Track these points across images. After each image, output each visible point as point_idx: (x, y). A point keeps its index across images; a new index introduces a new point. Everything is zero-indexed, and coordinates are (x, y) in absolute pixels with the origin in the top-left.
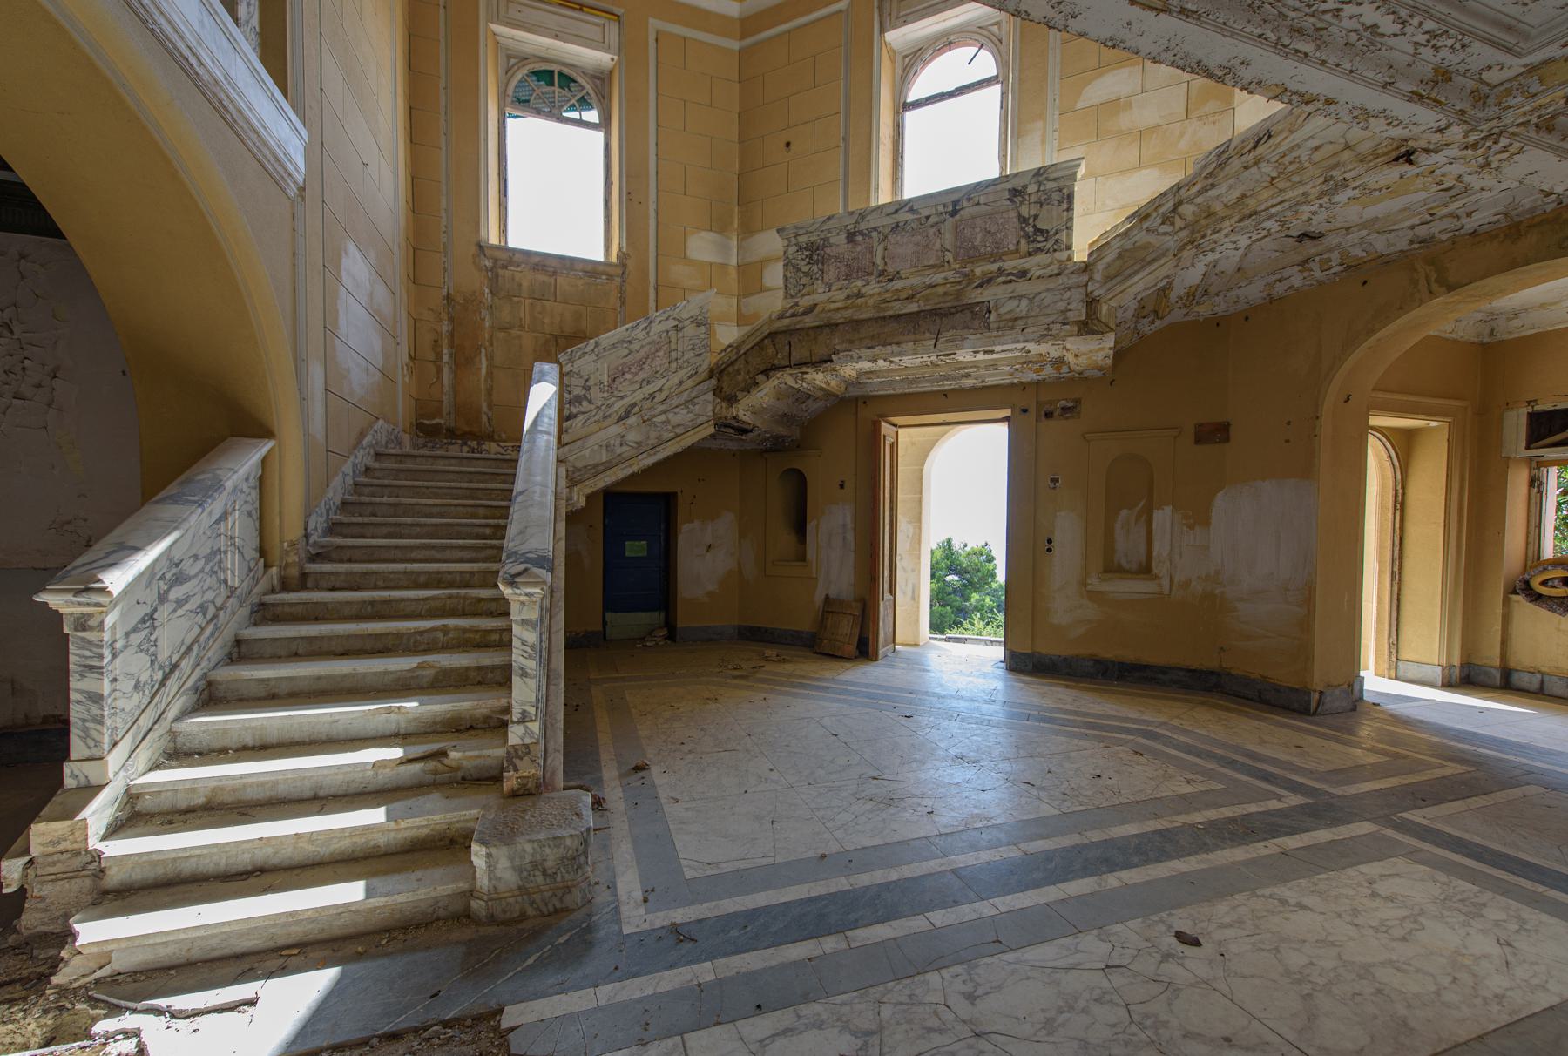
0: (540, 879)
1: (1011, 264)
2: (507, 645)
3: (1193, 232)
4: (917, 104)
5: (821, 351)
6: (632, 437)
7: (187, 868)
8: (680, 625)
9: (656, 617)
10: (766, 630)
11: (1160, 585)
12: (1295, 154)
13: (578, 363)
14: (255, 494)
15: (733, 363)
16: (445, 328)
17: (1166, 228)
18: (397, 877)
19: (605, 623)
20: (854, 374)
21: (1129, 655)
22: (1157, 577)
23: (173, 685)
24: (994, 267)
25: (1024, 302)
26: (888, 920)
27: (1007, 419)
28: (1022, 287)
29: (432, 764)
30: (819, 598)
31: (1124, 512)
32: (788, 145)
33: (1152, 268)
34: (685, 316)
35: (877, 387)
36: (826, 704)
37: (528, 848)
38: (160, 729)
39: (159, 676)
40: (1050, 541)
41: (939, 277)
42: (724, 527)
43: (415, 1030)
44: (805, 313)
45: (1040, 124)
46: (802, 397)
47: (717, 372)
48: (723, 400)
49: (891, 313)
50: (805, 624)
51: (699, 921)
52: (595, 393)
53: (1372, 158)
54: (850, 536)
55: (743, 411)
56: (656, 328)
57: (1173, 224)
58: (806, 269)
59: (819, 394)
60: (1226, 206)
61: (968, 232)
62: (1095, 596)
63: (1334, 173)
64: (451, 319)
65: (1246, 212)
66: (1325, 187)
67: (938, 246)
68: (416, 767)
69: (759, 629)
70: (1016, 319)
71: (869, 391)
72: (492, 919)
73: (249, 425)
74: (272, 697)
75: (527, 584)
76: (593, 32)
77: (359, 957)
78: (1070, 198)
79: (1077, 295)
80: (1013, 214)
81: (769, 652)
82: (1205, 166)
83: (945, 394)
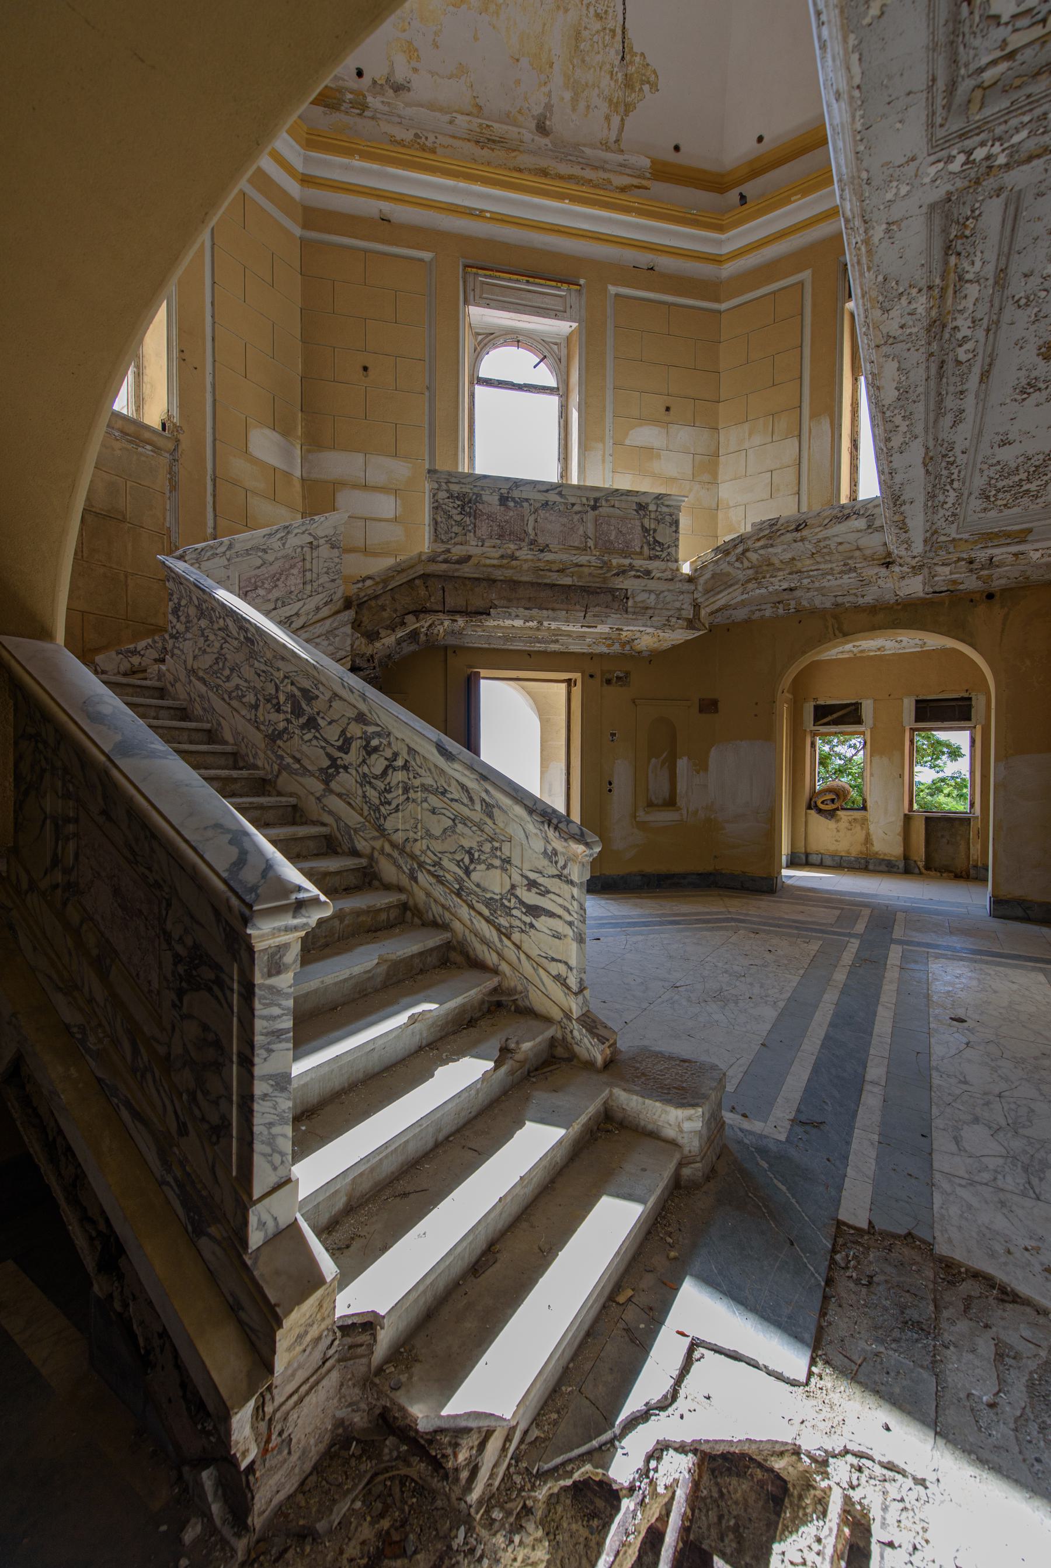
1: (638, 563)
3: (757, 573)
4: (488, 382)
5: (477, 603)
11: (681, 815)
12: (827, 542)
17: (737, 564)
21: (662, 868)
22: (679, 809)
24: (627, 562)
27: (569, 681)
28: (652, 585)
31: (653, 760)
33: (731, 590)
34: (320, 533)
40: (610, 784)
41: (583, 559)
45: (600, 445)
49: (548, 581)
53: (870, 559)
57: (742, 563)
58: (458, 518)
60: (781, 561)
61: (605, 527)
62: (642, 826)
63: (850, 562)
65: (794, 569)
66: (844, 568)
67: (581, 532)
70: (647, 608)
79: (687, 599)
80: (638, 523)
82: (761, 530)
83: (529, 654)
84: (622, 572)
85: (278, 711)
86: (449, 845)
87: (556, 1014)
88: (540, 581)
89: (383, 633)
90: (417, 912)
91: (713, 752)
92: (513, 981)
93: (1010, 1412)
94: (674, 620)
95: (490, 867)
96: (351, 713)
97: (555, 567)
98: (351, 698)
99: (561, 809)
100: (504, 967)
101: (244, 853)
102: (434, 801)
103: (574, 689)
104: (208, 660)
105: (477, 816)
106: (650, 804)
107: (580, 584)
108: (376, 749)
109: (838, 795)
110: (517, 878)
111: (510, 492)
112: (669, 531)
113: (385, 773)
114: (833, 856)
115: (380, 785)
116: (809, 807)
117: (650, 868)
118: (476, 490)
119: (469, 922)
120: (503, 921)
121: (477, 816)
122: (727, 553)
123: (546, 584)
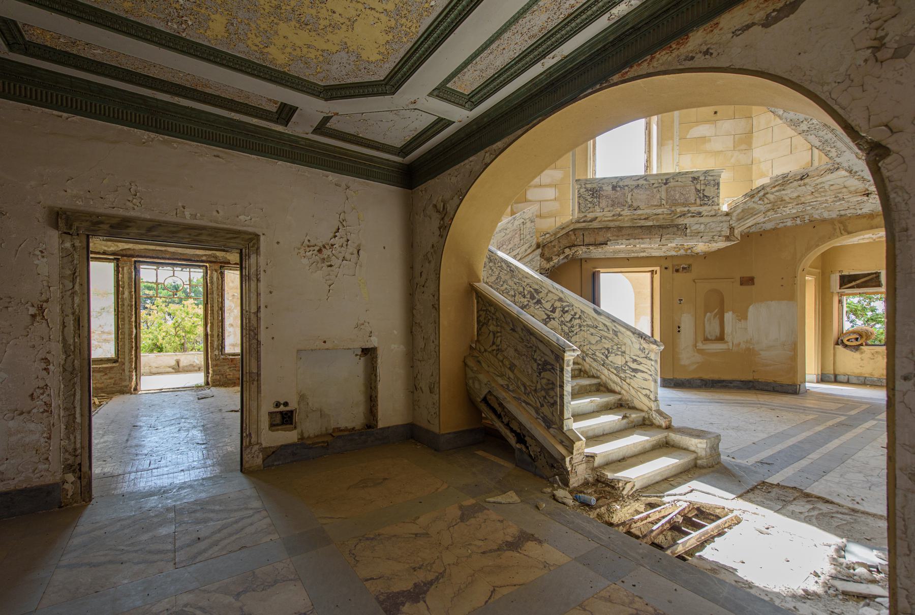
1: (693, 209)
5: (601, 239)
17: (760, 202)
21: (716, 377)
24: (686, 209)
25: (703, 226)
28: (702, 220)
41: (659, 211)
44: (591, 221)
45: (671, 142)
61: (672, 193)
62: (700, 351)
67: (658, 197)
78: (718, 184)
79: (726, 225)
80: (693, 187)
84: (683, 215)
85: (524, 297)
86: (599, 347)
87: (646, 409)
90: (586, 372)
91: (751, 309)
92: (626, 396)
94: (716, 238)
95: (616, 355)
96: (556, 298)
97: (643, 217)
98: (557, 292)
99: (649, 333)
100: (623, 392)
101: (558, 339)
102: (592, 330)
103: (655, 276)
104: (493, 279)
105: (611, 335)
106: (706, 339)
108: (567, 311)
109: (861, 336)
110: (628, 359)
111: (617, 184)
112: (713, 189)
113: (571, 320)
114: (858, 377)
115: (569, 325)
116: (837, 344)
117: (706, 376)
119: (607, 375)
120: (622, 375)
121: (611, 335)
122: (752, 196)
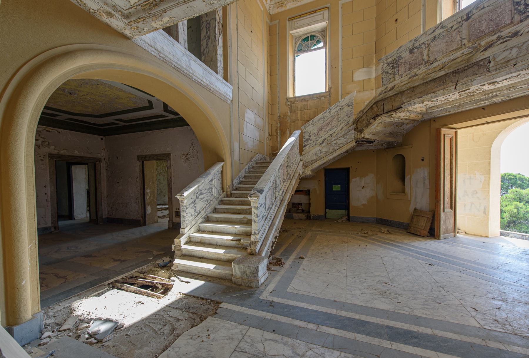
0: (246, 276)
2: (250, 214)
5: (397, 104)
6: (324, 150)
7: (193, 253)
8: (351, 215)
9: (344, 212)
10: (388, 220)
13: (307, 129)
14: (220, 175)
15: (361, 117)
16: (278, 125)
18: (221, 266)
19: (326, 213)
20: (424, 109)
23: (199, 216)
25: (515, 51)
26: (339, 329)
29: (238, 242)
30: (411, 209)
32: (396, 20)
34: (343, 104)
35: (438, 113)
36: (391, 252)
37: (242, 267)
38: (197, 224)
39: (197, 214)
42: (370, 179)
43: (207, 299)
46: (399, 124)
47: (356, 122)
48: (358, 132)
49: (430, 79)
50: (405, 220)
51: (279, 303)
52: (313, 138)
54: (427, 182)
55: (367, 134)
56: (333, 111)
58: (390, 72)
59: (407, 121)
64: (280, 122)
68: (234, 242)
69: (385, 220)
70: (508, 61)
71: (435, 115)
72: (235, 283)
73: (220, 159)
74: (218, 221)
75: (254, 197)
76: (320, 17)
77: (210, 281)
81: (383, 229)
83: (483, 108)
88: (425, 81)
89: (364, 129)
93: (165, 316)
107: (450, 71)
118: (398, 55)
123: (430, 81)
